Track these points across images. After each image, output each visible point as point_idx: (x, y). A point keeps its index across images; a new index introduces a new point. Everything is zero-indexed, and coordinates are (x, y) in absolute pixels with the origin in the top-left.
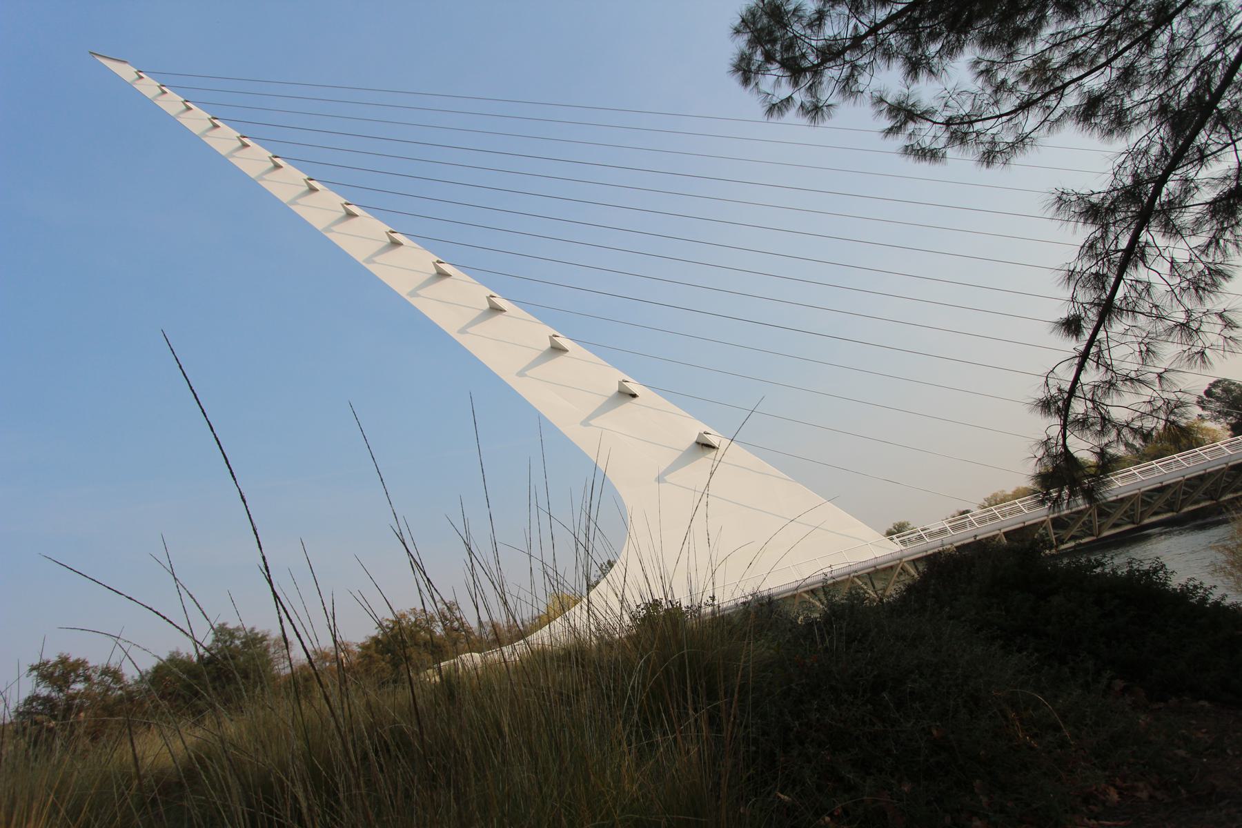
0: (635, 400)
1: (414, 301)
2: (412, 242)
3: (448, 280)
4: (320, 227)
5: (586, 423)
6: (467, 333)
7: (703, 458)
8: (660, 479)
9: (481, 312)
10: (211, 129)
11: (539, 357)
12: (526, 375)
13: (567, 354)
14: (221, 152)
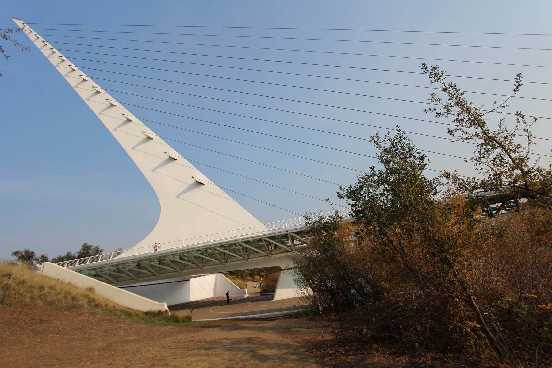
0: (175, 161)
1: (100, 117)
2: (122, 106)
3: (114, 107)
4: (54, 65)
5: (153, 170)
6: (155, 172)
7: (198, 188)
8: (178, 197)
9: (164, 160)
10: (44, 46)
11: (188, 188)
12: (102, 114)
13: (153, 140)
14: (38, 47)
